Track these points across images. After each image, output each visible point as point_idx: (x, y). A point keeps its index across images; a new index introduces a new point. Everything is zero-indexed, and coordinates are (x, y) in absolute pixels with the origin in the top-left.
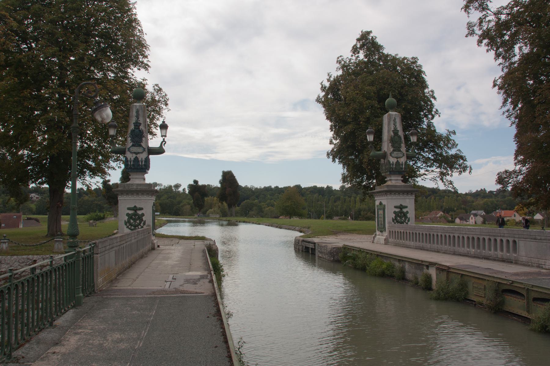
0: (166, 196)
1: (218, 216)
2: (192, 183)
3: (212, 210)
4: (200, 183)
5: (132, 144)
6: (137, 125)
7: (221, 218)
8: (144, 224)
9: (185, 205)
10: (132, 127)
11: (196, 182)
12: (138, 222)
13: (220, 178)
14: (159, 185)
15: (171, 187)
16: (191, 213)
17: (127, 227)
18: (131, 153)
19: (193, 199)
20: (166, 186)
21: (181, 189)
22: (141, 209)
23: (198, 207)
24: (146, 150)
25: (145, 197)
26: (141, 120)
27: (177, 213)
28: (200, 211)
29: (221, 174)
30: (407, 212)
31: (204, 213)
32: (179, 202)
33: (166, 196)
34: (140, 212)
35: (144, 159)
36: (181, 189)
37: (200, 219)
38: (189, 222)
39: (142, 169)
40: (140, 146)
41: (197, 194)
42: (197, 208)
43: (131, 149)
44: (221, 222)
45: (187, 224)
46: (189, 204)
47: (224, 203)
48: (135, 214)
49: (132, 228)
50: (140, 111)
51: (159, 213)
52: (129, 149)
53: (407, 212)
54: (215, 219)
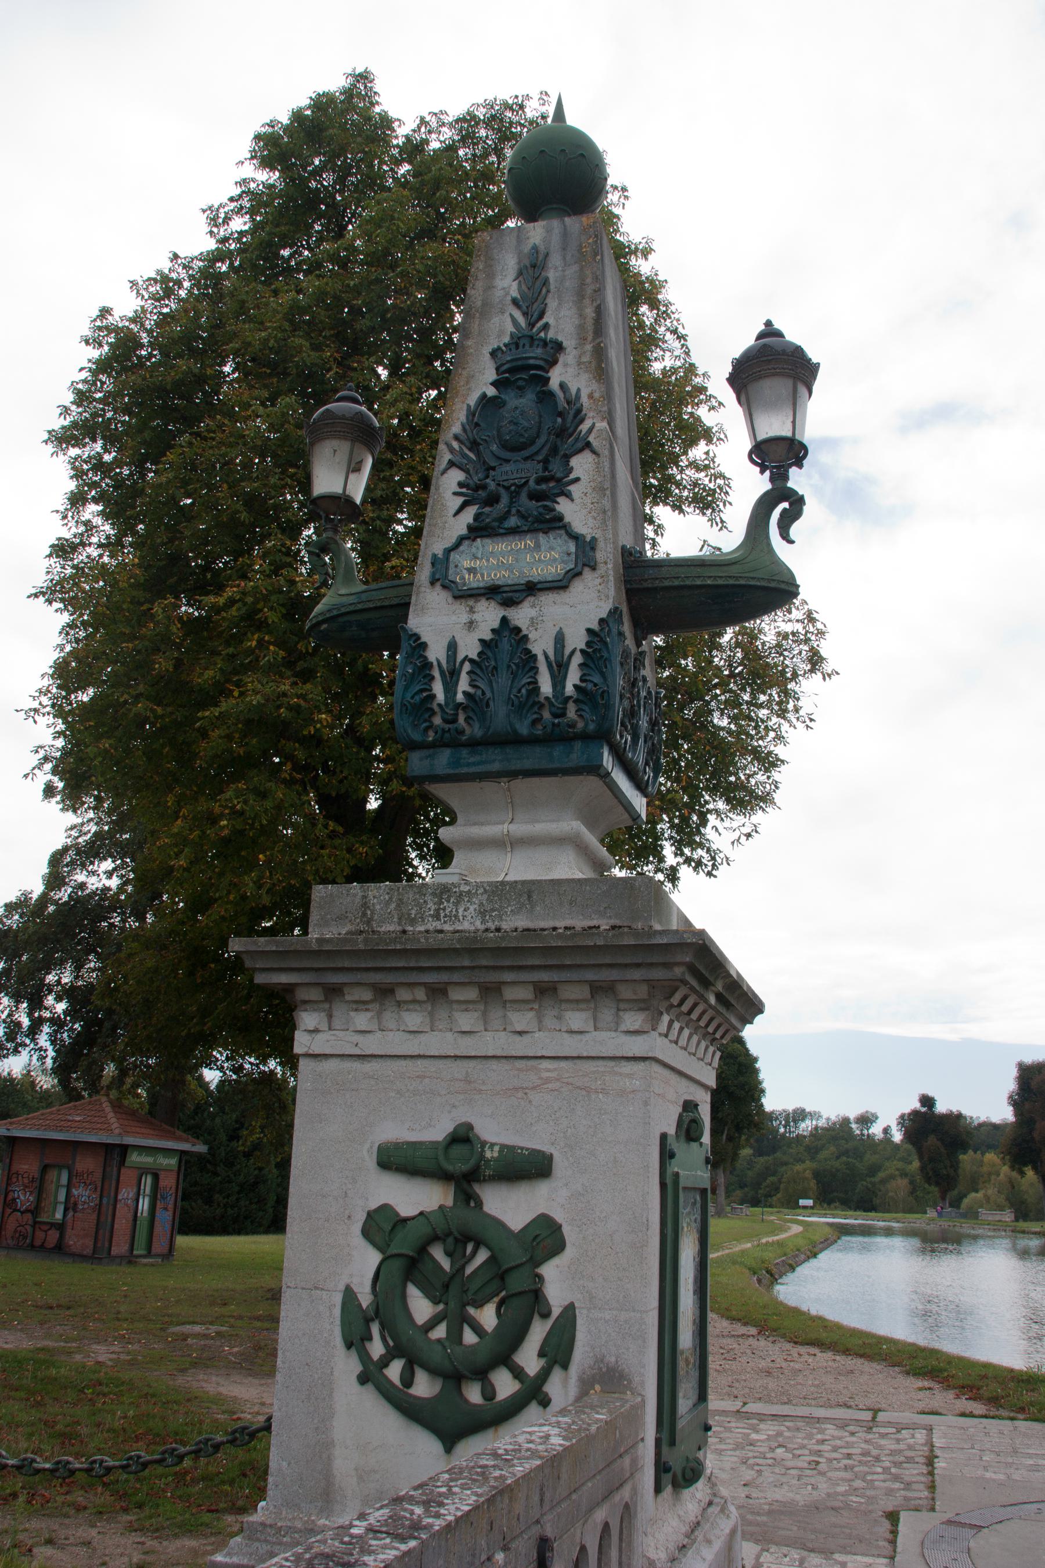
0: (832, 1149)
1: (1008, 1216)
2: (916, 1105)
3: (979, 1195)
4: (941, 1108)
5: (469, 515)
6: (525, 367)
7: (1022, 1225)
8: (558, 1352)
9: (892, 1177)
10: (481, 379)
11: (927, 1101)
12: (488, 1317)
13: (1010, 1085)
14: (812, 1115)
15: (846, 1121)
16: (915, 1204)
17: (370, 1375)
18: (464, 595)
19: (921, 1158)
20: (833, 1118)
21: (876, 1130)
22: (531, 1168)
23: (937, 1184)
24: (606, 556)
25: (574, 1031)
26: (562, 321)
27: (866, 1204)
28: (943, 1199)
29: (1014, 1072)
30: (546, 1238)
31: (956, 1204)
32: (873, 1170)
33: (832, 1149)
34: (510, 1207)
35: (576, 640)
36: (876, 1130)
37: (944, 1223)
38: (908, 1233)
39: (561, 736)
40: (554, 523)
41: (932, 1140)
42: (934, 1189)
43: (463, 560)
44: (1023, 1242)
45: (897, 1242)
46: (904, 1174)
47: (1030, 1173)
48: (462, 1231)
49: (424, 1387)
50: (555, 260)
51: (809, 1202)
52: (441, 565)
53: (546, 1238)
54: (998, 1227)
